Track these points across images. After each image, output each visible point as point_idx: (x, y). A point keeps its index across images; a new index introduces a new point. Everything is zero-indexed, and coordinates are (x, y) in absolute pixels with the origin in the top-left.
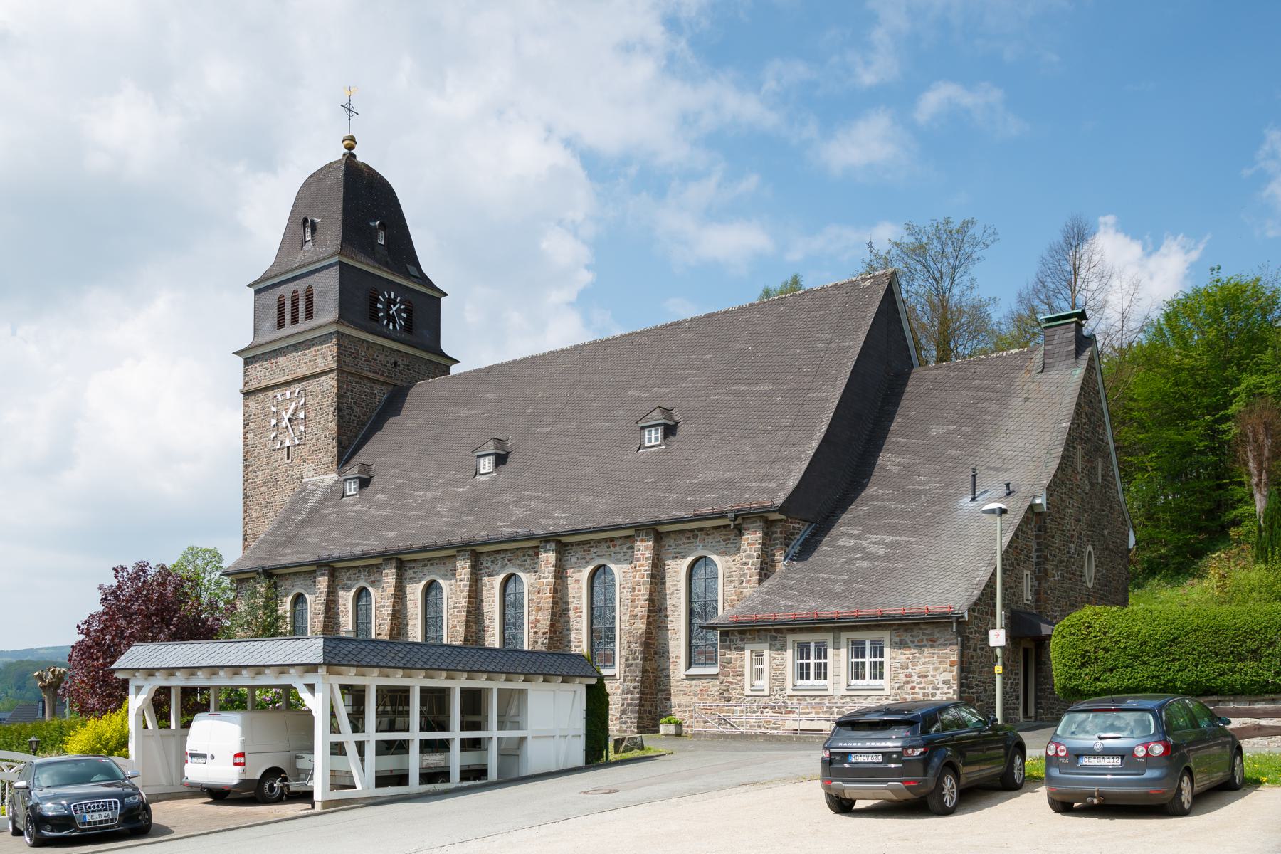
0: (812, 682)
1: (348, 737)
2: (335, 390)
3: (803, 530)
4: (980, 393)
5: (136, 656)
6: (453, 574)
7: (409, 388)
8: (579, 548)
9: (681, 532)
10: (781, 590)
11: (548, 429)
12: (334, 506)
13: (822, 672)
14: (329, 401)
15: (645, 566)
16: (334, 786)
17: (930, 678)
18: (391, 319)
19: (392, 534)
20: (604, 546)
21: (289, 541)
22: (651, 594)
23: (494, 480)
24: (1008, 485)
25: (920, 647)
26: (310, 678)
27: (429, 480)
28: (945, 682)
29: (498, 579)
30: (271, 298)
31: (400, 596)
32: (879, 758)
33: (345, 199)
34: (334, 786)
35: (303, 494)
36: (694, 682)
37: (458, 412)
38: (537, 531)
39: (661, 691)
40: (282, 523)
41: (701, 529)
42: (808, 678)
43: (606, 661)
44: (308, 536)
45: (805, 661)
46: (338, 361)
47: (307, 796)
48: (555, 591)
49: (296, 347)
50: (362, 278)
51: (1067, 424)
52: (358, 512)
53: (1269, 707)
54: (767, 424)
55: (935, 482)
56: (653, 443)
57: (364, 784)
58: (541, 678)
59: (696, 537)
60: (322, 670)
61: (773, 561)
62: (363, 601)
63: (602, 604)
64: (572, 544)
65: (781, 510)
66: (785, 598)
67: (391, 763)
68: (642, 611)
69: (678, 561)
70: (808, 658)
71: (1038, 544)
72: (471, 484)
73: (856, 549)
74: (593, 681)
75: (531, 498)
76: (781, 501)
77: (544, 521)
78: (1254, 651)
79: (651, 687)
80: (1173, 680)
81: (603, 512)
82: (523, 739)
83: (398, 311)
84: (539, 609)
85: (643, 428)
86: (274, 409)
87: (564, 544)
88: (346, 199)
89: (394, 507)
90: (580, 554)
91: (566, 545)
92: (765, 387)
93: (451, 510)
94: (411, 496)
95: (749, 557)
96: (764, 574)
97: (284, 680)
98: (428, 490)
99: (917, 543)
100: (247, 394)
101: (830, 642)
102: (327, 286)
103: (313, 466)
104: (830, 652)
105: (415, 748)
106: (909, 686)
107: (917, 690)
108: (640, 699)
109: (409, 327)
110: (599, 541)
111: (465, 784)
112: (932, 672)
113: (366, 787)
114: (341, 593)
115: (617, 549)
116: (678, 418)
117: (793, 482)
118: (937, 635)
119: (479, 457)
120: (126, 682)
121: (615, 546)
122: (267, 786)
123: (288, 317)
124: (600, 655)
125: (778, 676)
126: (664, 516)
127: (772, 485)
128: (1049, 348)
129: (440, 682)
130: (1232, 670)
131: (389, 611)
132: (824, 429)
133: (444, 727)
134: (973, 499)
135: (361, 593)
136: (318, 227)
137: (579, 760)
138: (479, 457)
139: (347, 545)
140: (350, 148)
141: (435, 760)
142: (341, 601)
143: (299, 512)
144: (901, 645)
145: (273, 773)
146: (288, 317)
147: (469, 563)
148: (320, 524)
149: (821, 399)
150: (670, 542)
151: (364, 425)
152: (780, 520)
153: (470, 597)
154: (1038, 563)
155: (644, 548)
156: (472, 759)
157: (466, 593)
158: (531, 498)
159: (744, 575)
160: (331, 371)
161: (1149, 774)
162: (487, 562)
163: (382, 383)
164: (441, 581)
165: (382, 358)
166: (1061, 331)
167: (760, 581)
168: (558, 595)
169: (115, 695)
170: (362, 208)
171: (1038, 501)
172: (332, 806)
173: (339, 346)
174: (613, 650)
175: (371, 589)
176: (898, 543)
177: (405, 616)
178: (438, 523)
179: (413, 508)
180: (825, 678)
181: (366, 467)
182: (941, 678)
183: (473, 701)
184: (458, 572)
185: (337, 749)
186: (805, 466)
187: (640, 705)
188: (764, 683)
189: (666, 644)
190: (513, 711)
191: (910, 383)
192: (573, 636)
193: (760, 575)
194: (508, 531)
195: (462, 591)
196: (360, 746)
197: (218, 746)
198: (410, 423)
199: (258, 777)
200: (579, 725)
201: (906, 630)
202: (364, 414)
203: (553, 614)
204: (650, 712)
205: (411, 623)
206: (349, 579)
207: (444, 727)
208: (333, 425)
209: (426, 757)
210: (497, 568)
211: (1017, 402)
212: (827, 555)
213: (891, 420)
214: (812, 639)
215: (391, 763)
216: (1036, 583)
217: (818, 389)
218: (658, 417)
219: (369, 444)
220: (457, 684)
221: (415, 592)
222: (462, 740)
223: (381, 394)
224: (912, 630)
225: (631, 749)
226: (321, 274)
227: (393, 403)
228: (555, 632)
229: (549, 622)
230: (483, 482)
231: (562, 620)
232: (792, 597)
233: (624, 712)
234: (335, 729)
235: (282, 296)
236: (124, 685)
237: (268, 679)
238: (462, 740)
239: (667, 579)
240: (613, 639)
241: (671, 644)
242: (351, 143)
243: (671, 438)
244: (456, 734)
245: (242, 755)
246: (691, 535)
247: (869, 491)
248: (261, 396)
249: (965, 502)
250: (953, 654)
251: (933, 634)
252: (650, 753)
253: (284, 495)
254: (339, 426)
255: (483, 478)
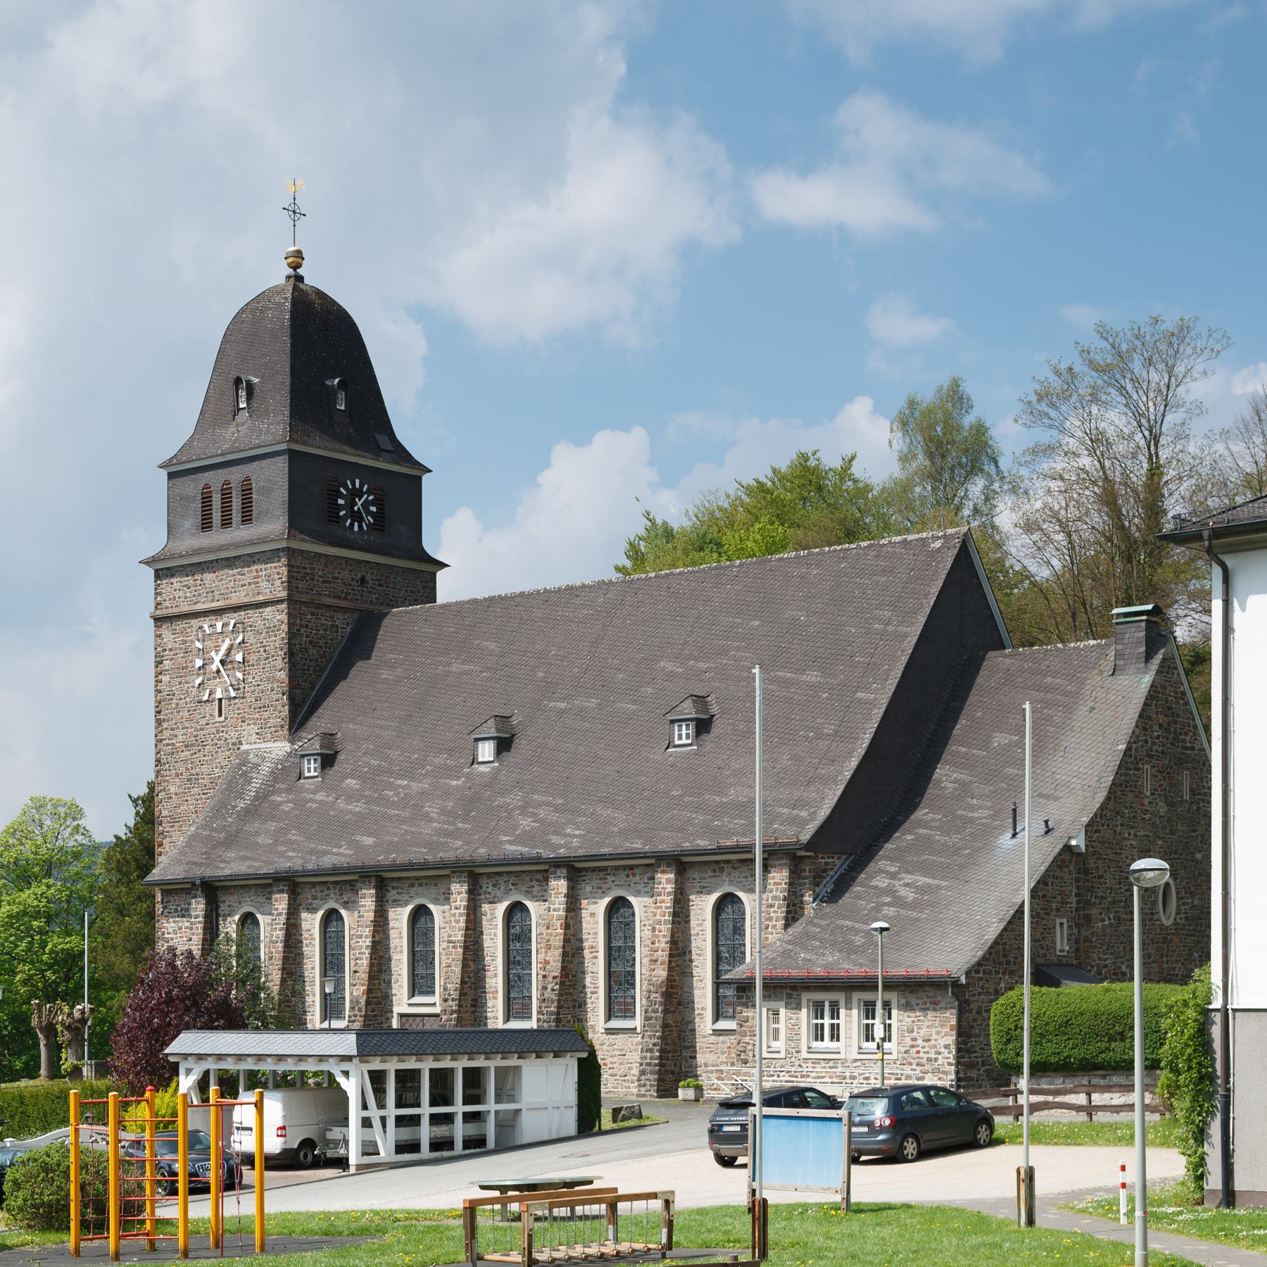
0: (827, 1044)
1: (374, 1113)
2: (285, 627)
3: (838, 864)
4: (1049, 696)
5: (186, 1043)
6: (446, 898)
7: (383, 616)
8: (594, 875)
9: (707, 863)
10: (801, 942)
11: (563, 705)
12: (289, 790)
13: (835, 1036)
14: (278, 641)
15: (667, 902)
16: (364, 1154)
17: (933, 1042)
18: (357, 517)
19: (369, 841)
20: (623, 874)
21: (231, 840)
22: (672, 936)
23: (496, 772)
24: (1046, 822)
25: (924, 1010)
26: (346, 1066)
27: (412, 777)
28: (946, 1047)
29: (502, 907)
30: (192, 487)
31: (381, 924)
32: (738, 1128)
33: (294, 355)
34: (364, 1154)
35: (242, 769)
36: (721, 1038)
37: (449, 664)
38: (547, 854)
39: (687, 1047)
40: (219, 809)
41: (728, 862)
42: (822, 1040)
43: (626, 1011)
44: (257, 834)
45: (820, 1021)
46: (290, 588)
47: (342, 1163)
48: (567, 926)
49: (230, 563)
50: (316, 458)
51: (1122, 747)
52: (320, 802)
53: (1102, 1082)
54: (809, 729)
55: (988, 808)
56: (684, 741)
57: (386, 1151)
58: (534, 1055)
59: (722, 870)
60: (355, 1061)
61: (802, 902)
62: (332, 928)
63: (620, 943)
64: (586, 869)
65: (809, 846)
66: (806, 949)
67: (406, 1134)
68: (663, 955)
69: (704, 897)
70: (822, 1018)
71: (1078, 888)
72: (468, 776)
73: (889, 891)
74: (585, 1055)
75: (540, 804)
76: (808, 837)
77: (555, 839)
78: (1121, 1034)
79: (674, 1044)
80: (1069, 1057)
81: (622, 832)
82: (518, 1111)
83: (366, 505)
84: (548, 947)
85: (672, 722)
86: (199, 645)
87: (579, 872)
88: (295, 354)
89: (370, 801)
90: (595, 883)
91: (580, 870)
92: (812, 677)
93: (443, 812)
94: (391, 786)
95: (775, 898)
96: (792, 916)
97: (324, 1067)
98: (412, 779)
99: (947, 887)
100: (159, 620)
101: (842, 1003)
102: (273, 481)
103: (255, 729)
104: (842, 1012)
105: (425, 1121)
106: (914, 1050)
107: (921, 1055)
108: (661, 1058)
109: (380, 523)
110: (617, 868)
111: (467, 1152)
112: (934, 1036)
113: (388, 1154)
114: (304, 915)
115: (637, 878)
116: (714, 709)
117: (824, 812)
118: (939, 998)
119: (477, 740)
120: (177, 1064)
121: (634, 875)
122: (302, 1154)
123: (217, 516)
124: (619, 1003)
125: (793, 1037)
126: (687, 845)
127: (804, 814)
128: (1120, 647)
129: (446, 1063)
130: (1107, 1049)
131: (368, 942)
132: (865, 745)
133: (448, 1101)
134: (1014, 836)
135: (332, 917)
136: (257, 391)
137: (572, 1128)
138: (477, 740)
139: (311, 852)
140: (296, 267)
141: (442, 1131)
142: (305, 925)
143: (240, 796)
144: (907, 1007)
145: (308, 1144)
146: (217, 516)
147: (465, 887)
148: (272, 818)
149: (868, 702)
150: (694, 874)
151: (322, 670)
152: (809, 857)
153: (467, 929)
154: (1077, 910)
155: (666, 881)
156: (473, 1129)
157: (462, 925)
158: (540, 804)
159: (770, 919)
160: (280, 601)
161: (881, 1137)
162: (487, 886)
163: (345, 610)
164: (431, 906)
165: (345, 575)
166: (1131, 628)
167: (786, 926)
168: (571, 931)
169: (165, 1074)
170: (314, 359)
171: (1074, 843)
172: (363, 1168)
173: (290, 567)
174: (634, 997)
175: (343, 912)
176: (929, 886)
177: (388, 948)
178: (427, 830)
179: (394, 805)
180: (838, 1040)
181: (328, 737)
182: (942, 1042)
183: (474, 1078)
184: (453, 897)
185: (366, 1123)
186: (839, 792)
187: (660, 1065)
188: (780, 1045)
189: (691, 994)
190: (509, 1086)
191: (982, 673)
192: (588, 980)
193: (786, 919)
194: (513, 849)
195: (457, 922)
196: (383, 1120)
197: (262, 1123)
198: (385, 674)
199: (296, 1146)
200: (571, 1097)
201: (911, 992)
202: (322, 656)
203: (565, 954)
204: (673, 1073)
205: (395, 957)
206: (315, 898)
207: (448, 1101)
208: (283, 675)
209: (434, 1128)
210: (499, 894)
211: (1083, 711)
212: (859, 898)
213: (955, 723)
214: (827, 997)
215: (406, 1134)
216: (1075, 931)
217: (867, 688)
218: (688, 709)
219: (331, 701)
220: (459, 1065)
221: (399, 918)
222: (464, 1114)
223: (345, 625)
224: (917, 992)
225: (629, 1118)
226: (264, 463)
227: (360, 641)
228: (567, 976)
229: (559, 965)
230: (482, 775)
231: (576, 960)
232: (814, 948)
233: (643, 1073)
234: (365, 1107)
235: (207, 487)
236: (175, 1069)
237: (310, 1066)
238: (464, 1114)
239: (692, 918)
240: (633, 985)
241: (697, 993)
242: (296, 259)
243: (704, 737)
244: (459, 1108)
245: (283, 1128)
246: (716, 867)
247: (920, 814)
248: (180, 625)
249: (1005, 840)
250: (951, 1017)
251: (935, 996)
252: (647, 1122)
253: (216, 766)
254: (292, 677)
255: (482, 768)
